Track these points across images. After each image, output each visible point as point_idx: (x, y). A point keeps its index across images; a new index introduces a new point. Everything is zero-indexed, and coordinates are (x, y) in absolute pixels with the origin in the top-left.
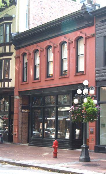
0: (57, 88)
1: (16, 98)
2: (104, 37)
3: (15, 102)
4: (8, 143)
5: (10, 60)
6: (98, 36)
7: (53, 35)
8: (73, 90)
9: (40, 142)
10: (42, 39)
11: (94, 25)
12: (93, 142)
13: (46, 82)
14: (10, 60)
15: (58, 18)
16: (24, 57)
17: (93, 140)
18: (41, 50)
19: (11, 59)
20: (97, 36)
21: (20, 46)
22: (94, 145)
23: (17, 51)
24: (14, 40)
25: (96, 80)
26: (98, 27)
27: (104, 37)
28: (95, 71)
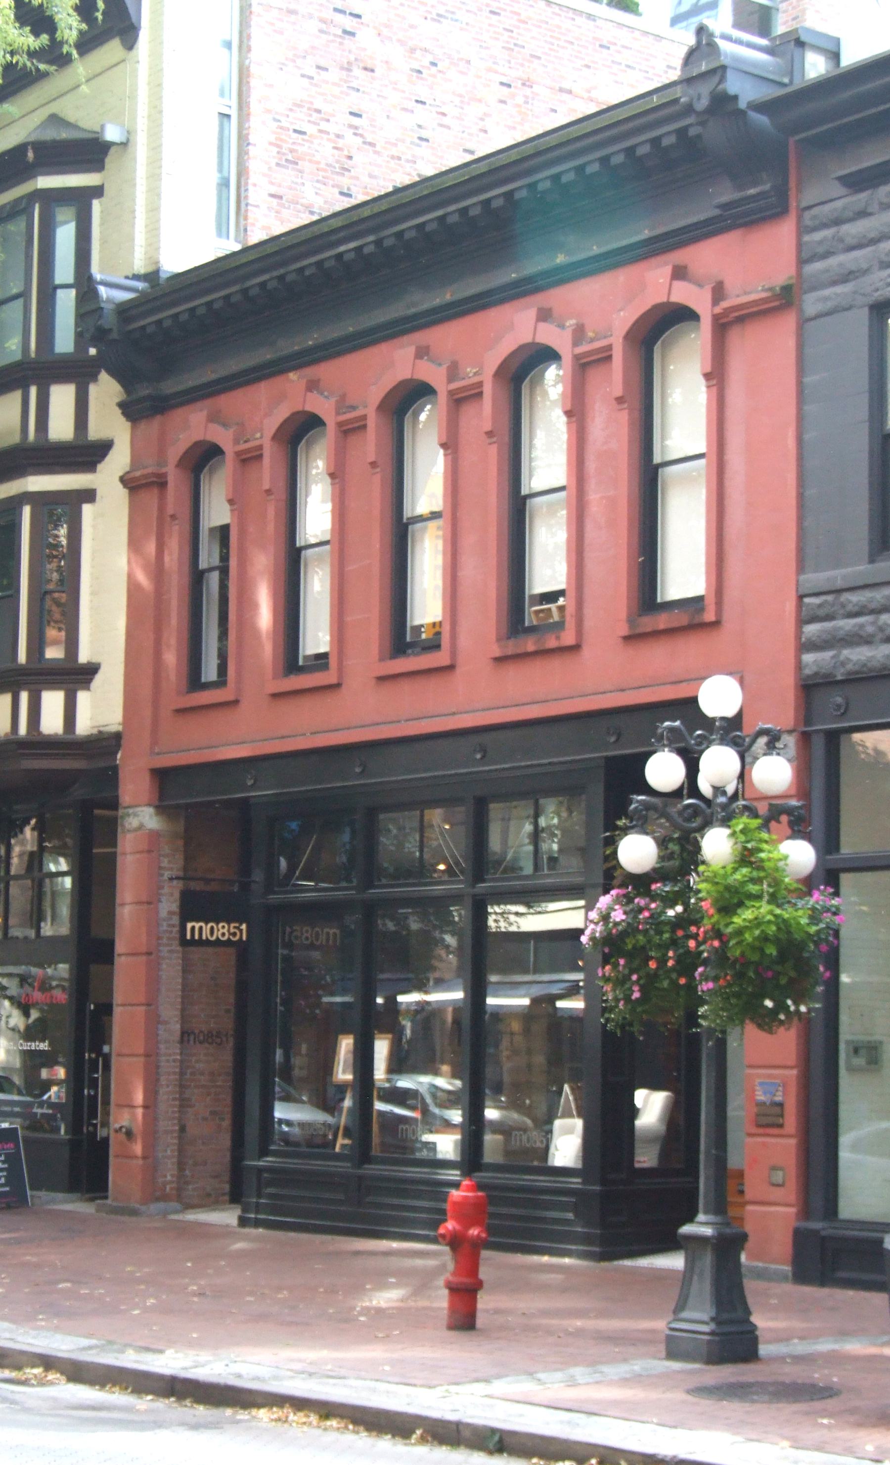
0: (487, 738)
5: (87, 508)
6: (826, 299)
12: (777, 1194)
14: (87, 508)
17: (778, 1177)
20: (811, 304)
22: (793, 1223)
26: (825, 226)
28: (801, 597)
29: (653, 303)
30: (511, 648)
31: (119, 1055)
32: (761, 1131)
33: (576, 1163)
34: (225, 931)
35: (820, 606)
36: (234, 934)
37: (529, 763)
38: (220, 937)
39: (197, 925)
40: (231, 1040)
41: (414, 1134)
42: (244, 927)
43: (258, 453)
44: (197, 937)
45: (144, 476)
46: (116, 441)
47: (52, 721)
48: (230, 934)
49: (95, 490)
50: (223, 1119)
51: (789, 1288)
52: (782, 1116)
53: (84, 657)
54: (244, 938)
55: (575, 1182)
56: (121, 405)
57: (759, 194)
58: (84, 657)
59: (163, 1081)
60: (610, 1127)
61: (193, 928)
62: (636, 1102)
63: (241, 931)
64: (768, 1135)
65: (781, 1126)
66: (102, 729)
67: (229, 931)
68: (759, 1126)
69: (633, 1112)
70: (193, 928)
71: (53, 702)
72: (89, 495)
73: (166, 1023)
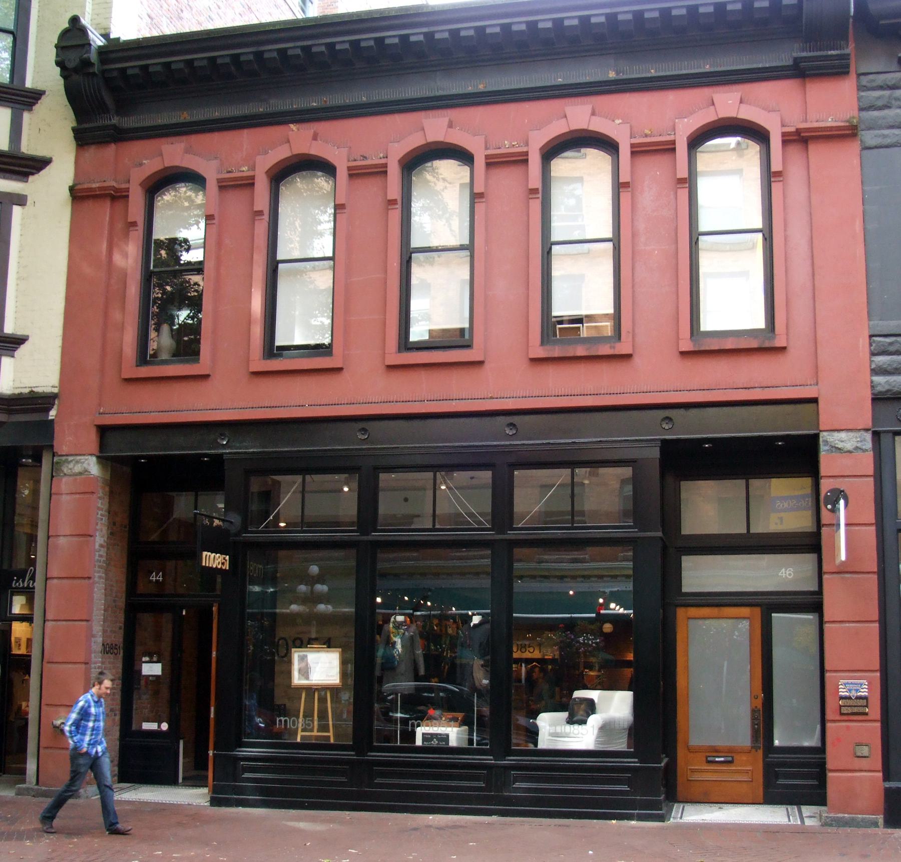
0: (516, 419)
1: (78, 468)
2: (462, 185)
3: (65, 498)
4: (302, 825)
5: (17, 210)
6: (885, 136)
7: (217, 114)
8: (664, 442)
9: (344, 779)
10: (362, 97)
11: (853, 75)
12: (864, 763)
13: (689, 363)
14: (17, 210)
15: (210, 26)
16: (283, 189)
17: (865, 751)
18: (487, 157)
19: (21, 200)
20: (869, 137)
21: (130, 122)
22: (882, 785)
23: (91, 152)
24: (96, 69)
25: (879, 389)
26: (881, 88)
27: (462, 185)
28: (871, 336)
30: (541, 353)
31: (49, 662)
32: (845, 718)
33: (597, 742)
35: (891, 344)
37: (545, 442)
40: (122, 651)
41: (294, 725)
42: (227, 557)
43: (251, 181)
45: (100, 188)
46: (54, 159)
49: (26, 196)
50: (115, 715)
51: (881, 831)
56: (74, 129)
57: (837, 55)
64: (850, 721)
66: (35, 390)
68: (841, 714)
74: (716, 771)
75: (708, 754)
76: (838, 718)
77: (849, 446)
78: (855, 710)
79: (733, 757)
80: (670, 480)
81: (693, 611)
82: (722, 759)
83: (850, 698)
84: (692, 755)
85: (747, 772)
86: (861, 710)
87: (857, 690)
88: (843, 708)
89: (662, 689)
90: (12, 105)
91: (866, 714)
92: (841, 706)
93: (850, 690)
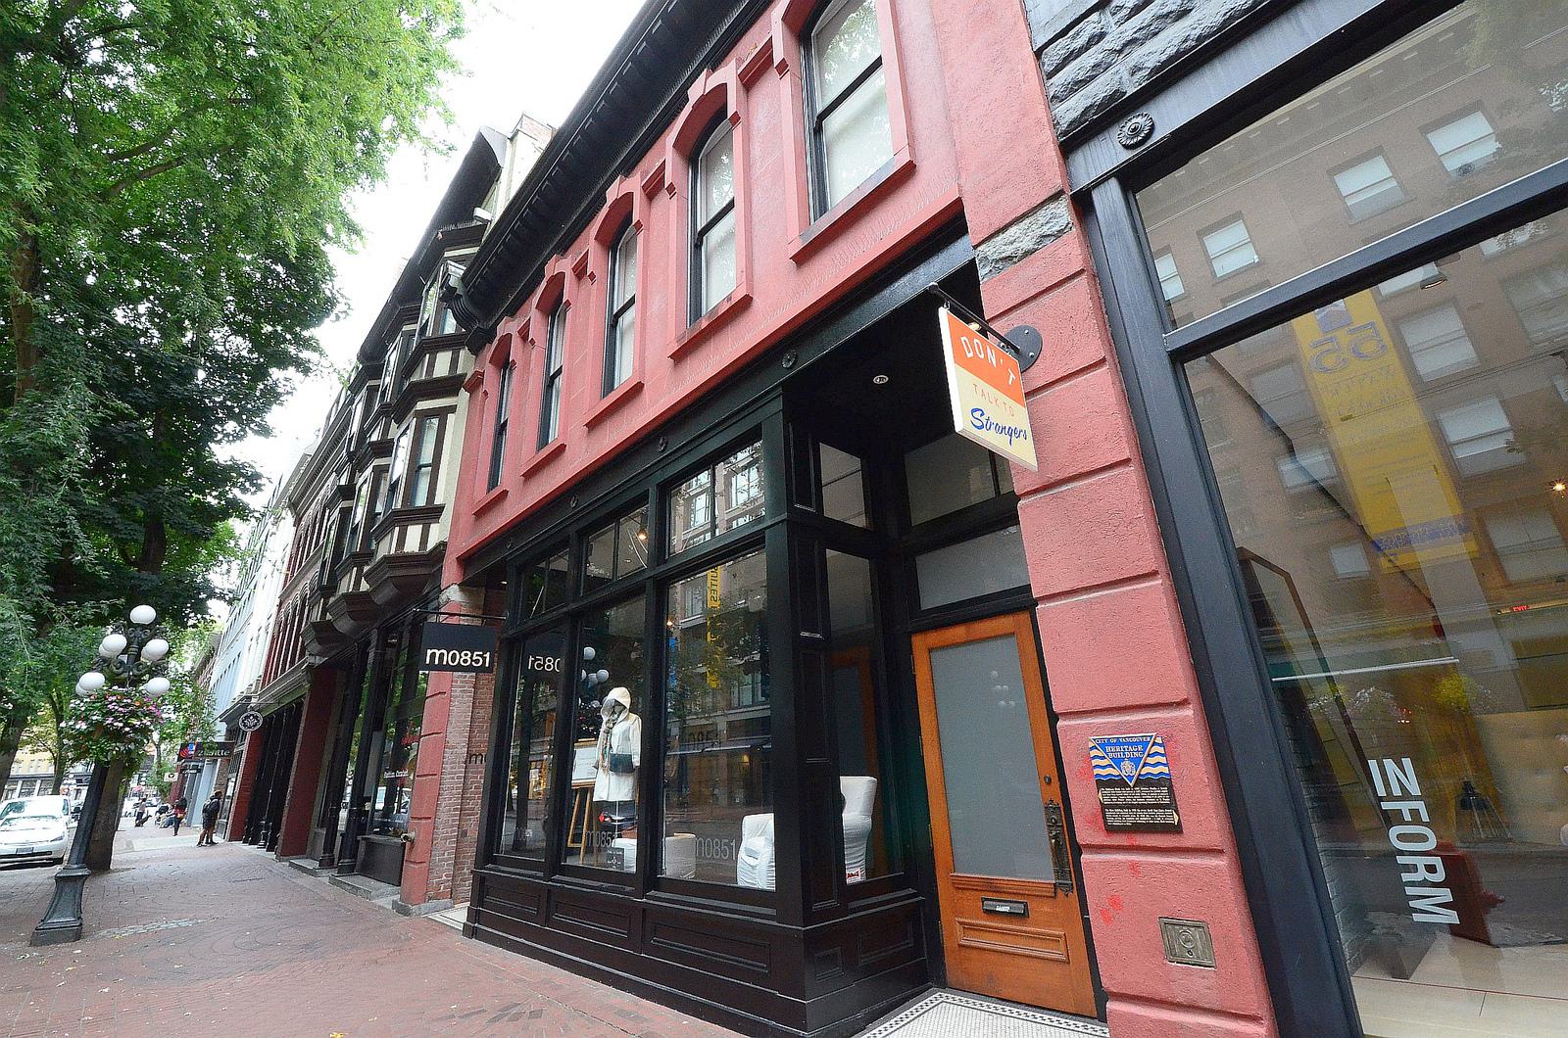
29: (847, 801)
34: (468, 658)
36: (477, 661)
38: (462, 663)
39: (438, 653)
42: (488, 655)
44: (437, 662)
47: (412, 545)
48: (472, 661)
52: (1173, 805)
53: (438, 501)
54: (487, 665)
55: (766, 917)
58: (438, 501)
59: (446, 794)
60: (809, 838)
61: (433, 654)
62: (844, 815)
63: (484, 659)
65: (1176, 829)
67: (471, 658)
68: (1111, 830)
69: (839, 803)
70: (433, 654)
71: (414, 532)
72: (452, 409)
73: (453, 747)
74: (1002, 932)
75: (984, 895)
76: (1101, 838)
77: (1027, 244)
78: (1144, 817)
79: (1026, 906)
80: (780, 390)
81: (934, 638)
82: (1006, 909)
83: (1121, 783)
84: (960, 894)
85: (1055, 939)
86: (1160, 817)
87: (1136, 761)
88: (1109, 812)
89: (396, 701)
90: (1342, 775)
91: (1176, 829)
92: (1103, 807)
93: (1118, 762)
